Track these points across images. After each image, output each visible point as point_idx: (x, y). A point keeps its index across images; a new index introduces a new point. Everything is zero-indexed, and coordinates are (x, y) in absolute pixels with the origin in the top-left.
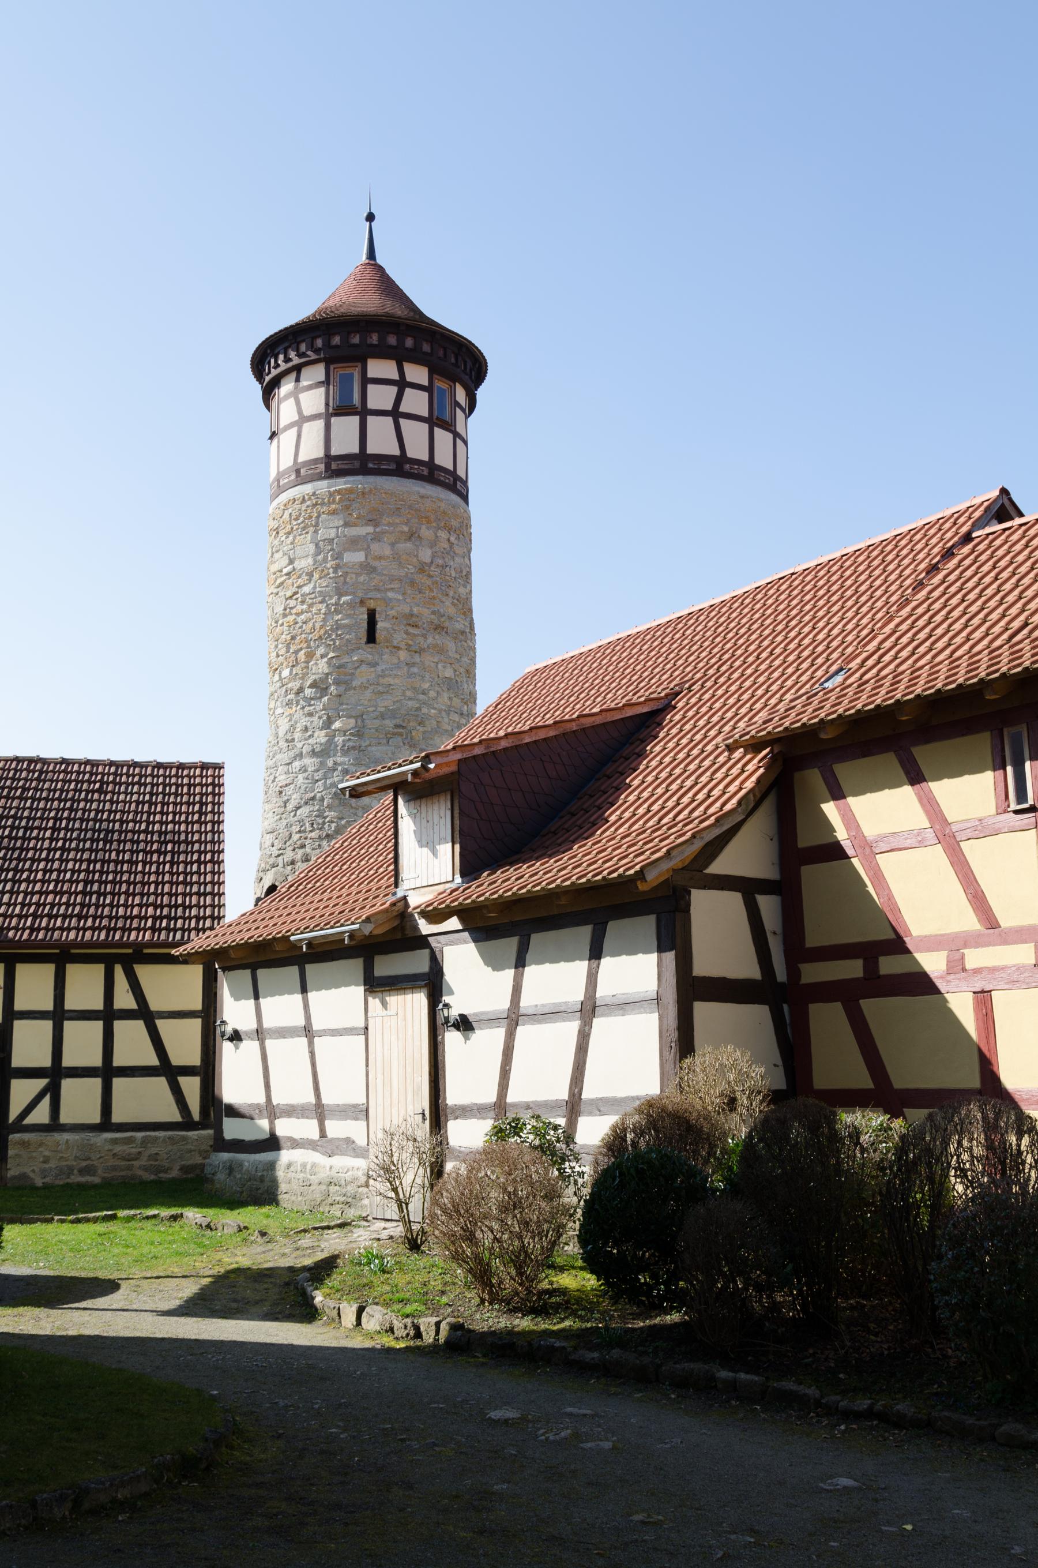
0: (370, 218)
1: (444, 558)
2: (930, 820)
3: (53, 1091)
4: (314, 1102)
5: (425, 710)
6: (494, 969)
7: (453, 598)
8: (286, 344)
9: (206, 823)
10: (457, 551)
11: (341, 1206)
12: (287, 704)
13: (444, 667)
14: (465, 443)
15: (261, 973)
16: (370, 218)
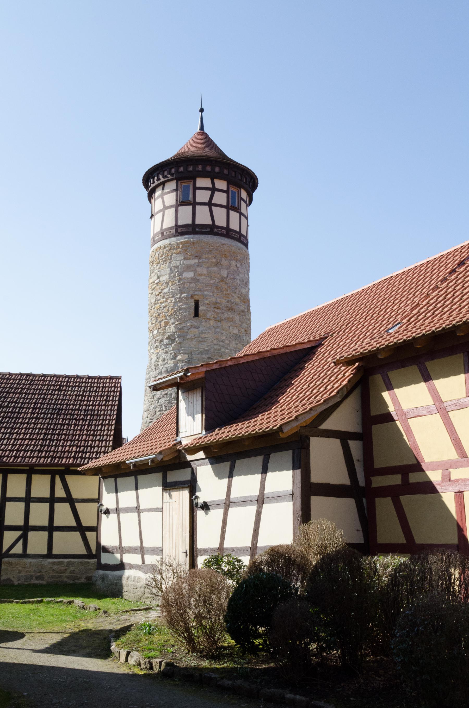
0: (202, 110)
1: (233, 275)
2: (434, 401)
3: (24, 537)
4: (140, 546)
5: (223, 350)
6: (219, 479)
7: (238, 294)
8: (158, 172)
9: (108, 406)
10: (241, 271)
11: (150, 599)
12: (156, 348)
13: (233, 329)
14: (247, 218)
15: (119, 480)
16: (202, 110)
